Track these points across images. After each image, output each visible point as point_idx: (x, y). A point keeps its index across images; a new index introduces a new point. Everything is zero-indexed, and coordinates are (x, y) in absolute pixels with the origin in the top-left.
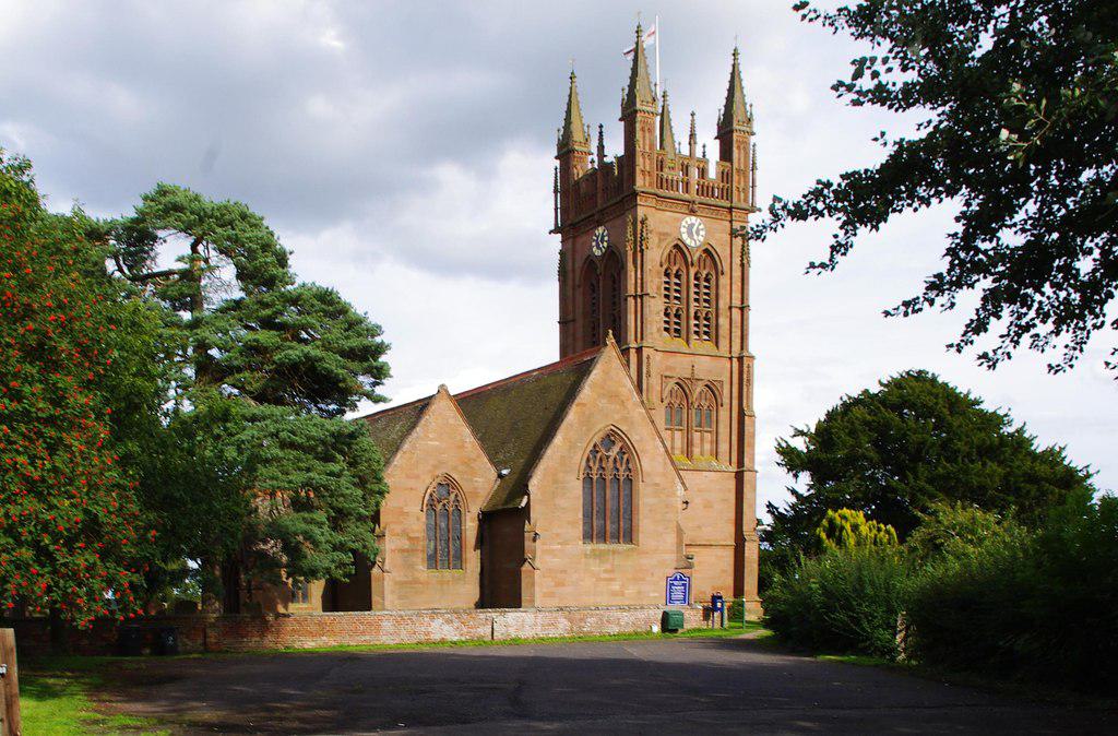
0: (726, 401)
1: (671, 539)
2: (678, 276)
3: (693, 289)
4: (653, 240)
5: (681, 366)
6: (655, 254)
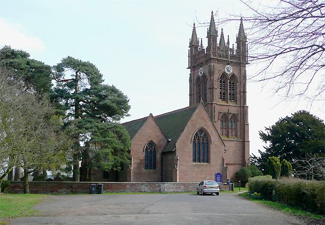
0: (239, 119)
1: (220, 161)
2: (224, 82)
3: (229, 87)
4: (216, 72)
5: (225, 110)
6: (217, 76)
